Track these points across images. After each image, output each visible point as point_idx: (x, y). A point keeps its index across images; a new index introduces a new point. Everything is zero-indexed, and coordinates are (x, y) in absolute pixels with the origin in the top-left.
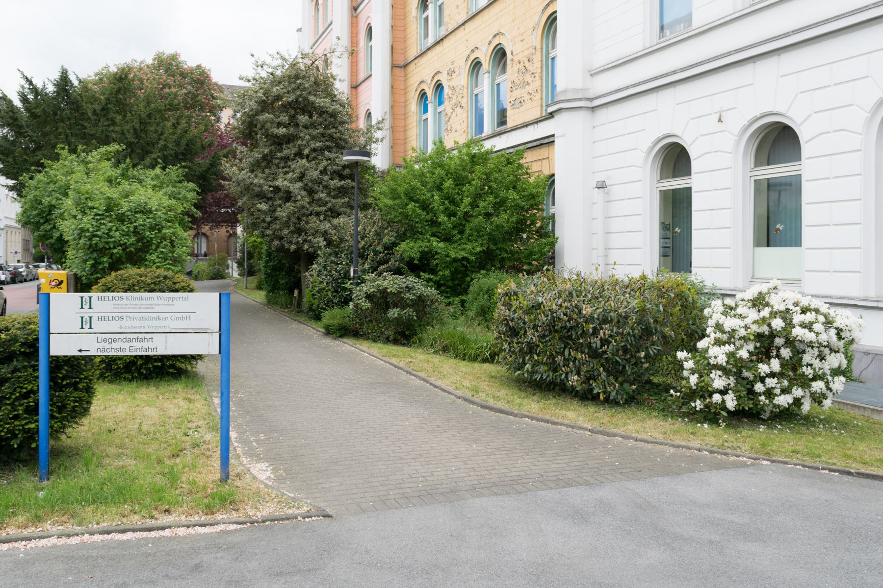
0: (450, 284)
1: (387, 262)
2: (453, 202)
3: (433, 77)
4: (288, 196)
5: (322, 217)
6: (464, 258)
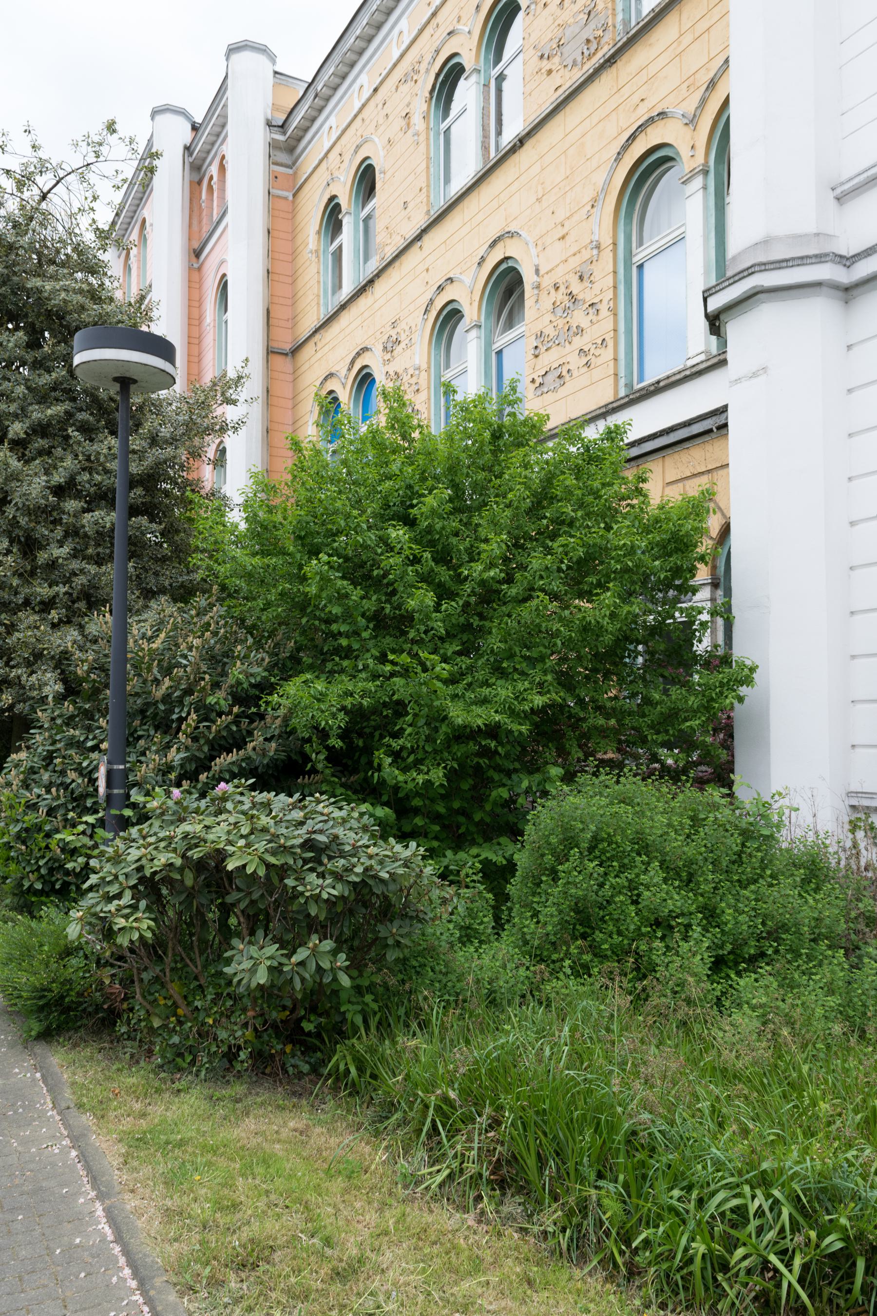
0: (441, 809)
1: (240, 744)
2: (443, 557)
3: (353, 362)
6: (493, 731)
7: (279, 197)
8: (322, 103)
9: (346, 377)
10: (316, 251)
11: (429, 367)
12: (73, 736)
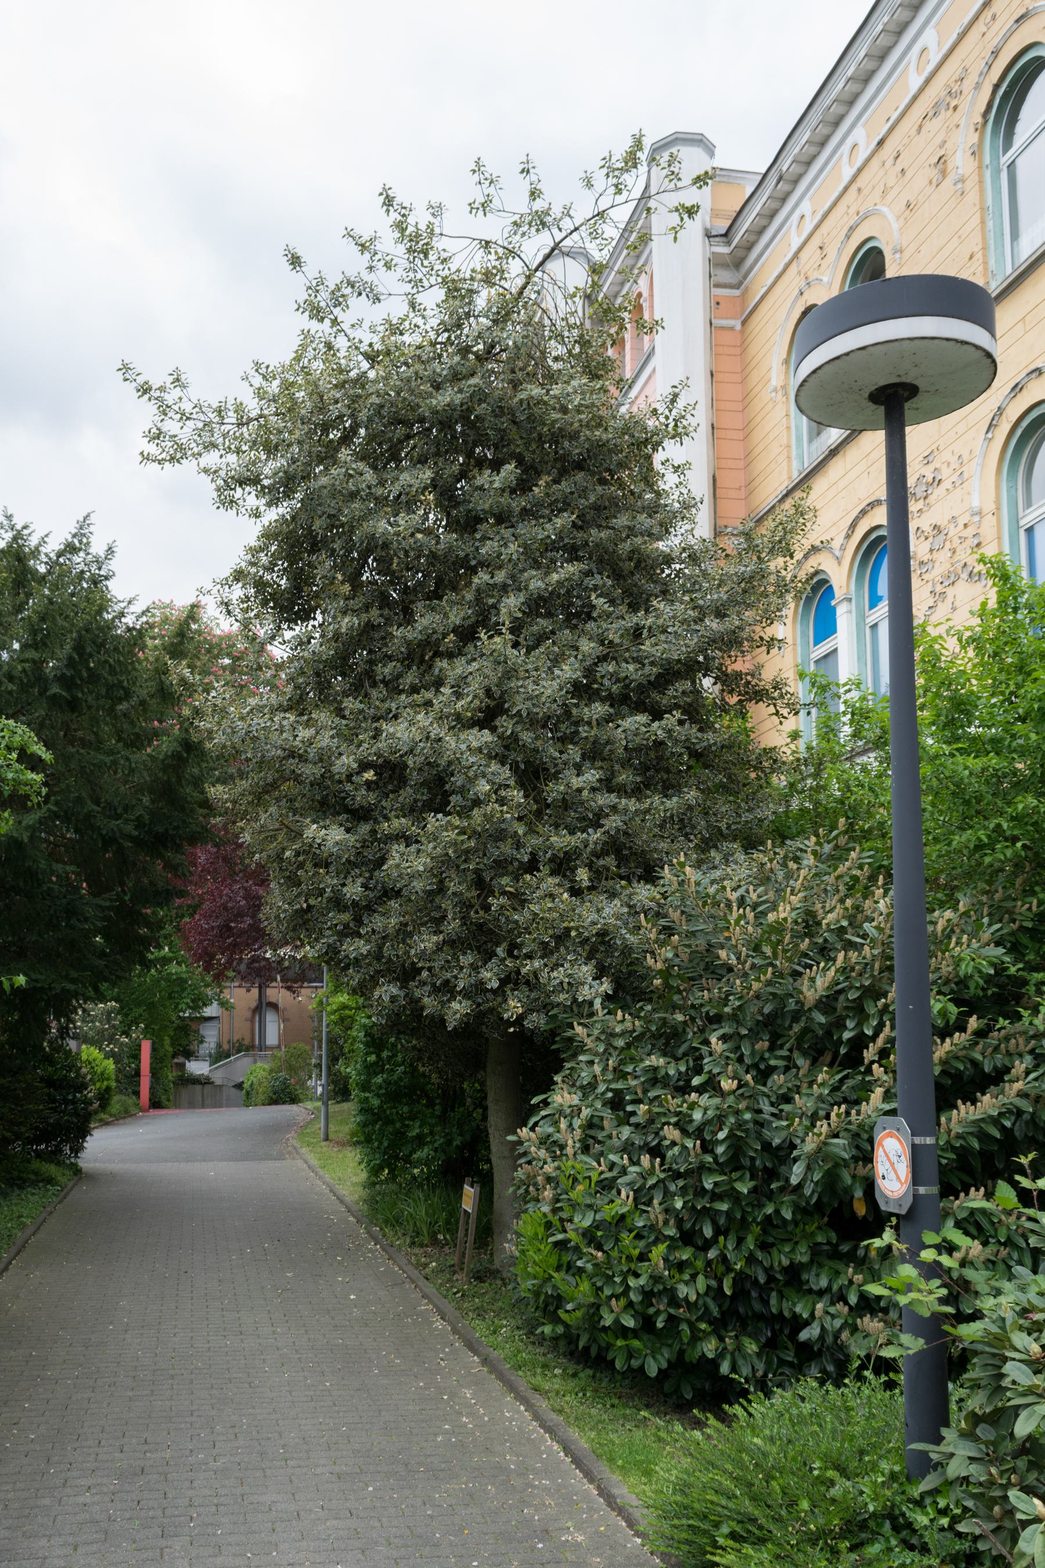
3: (853, 526)
4: (438, 790)
5: (583, 875)
7: (722, 328)
9: (843, 548)
11: (998, 508)
12: (655, 1069)
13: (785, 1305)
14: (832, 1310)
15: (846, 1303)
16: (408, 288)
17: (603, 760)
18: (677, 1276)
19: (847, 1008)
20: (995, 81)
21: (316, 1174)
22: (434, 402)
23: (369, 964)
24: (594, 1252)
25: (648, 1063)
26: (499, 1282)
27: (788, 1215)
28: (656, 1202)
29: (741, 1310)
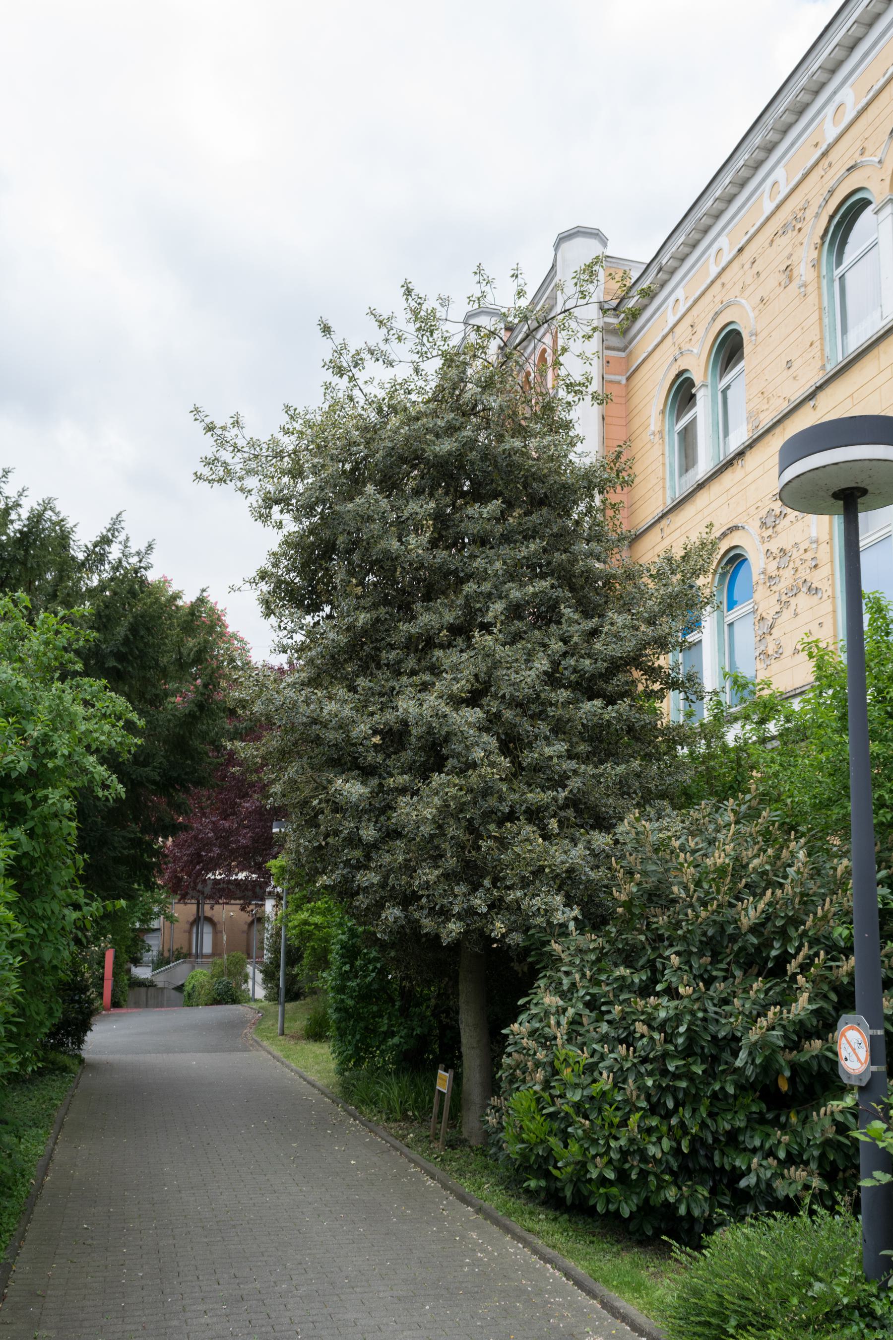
4: (436, 753)
7: (611, 382)
8: (665, 277)
10: (661, 432)
12: (623, 978)
13: (725, 1160)
14: (764, 1163)
15: (776, 1157)
16: (416, 357)
17: (564, 733)
18: (647, 1139)
19: (773, 932)
20: (831, 213)
21: (282, 1063)
22: (438, 449)
23: (375, 892)
24: (583, 1121)
25: (618, 973)
26: (468, 1149)
27: (731, 1090)
28: (630, 1081)
29: (690, 1165)
